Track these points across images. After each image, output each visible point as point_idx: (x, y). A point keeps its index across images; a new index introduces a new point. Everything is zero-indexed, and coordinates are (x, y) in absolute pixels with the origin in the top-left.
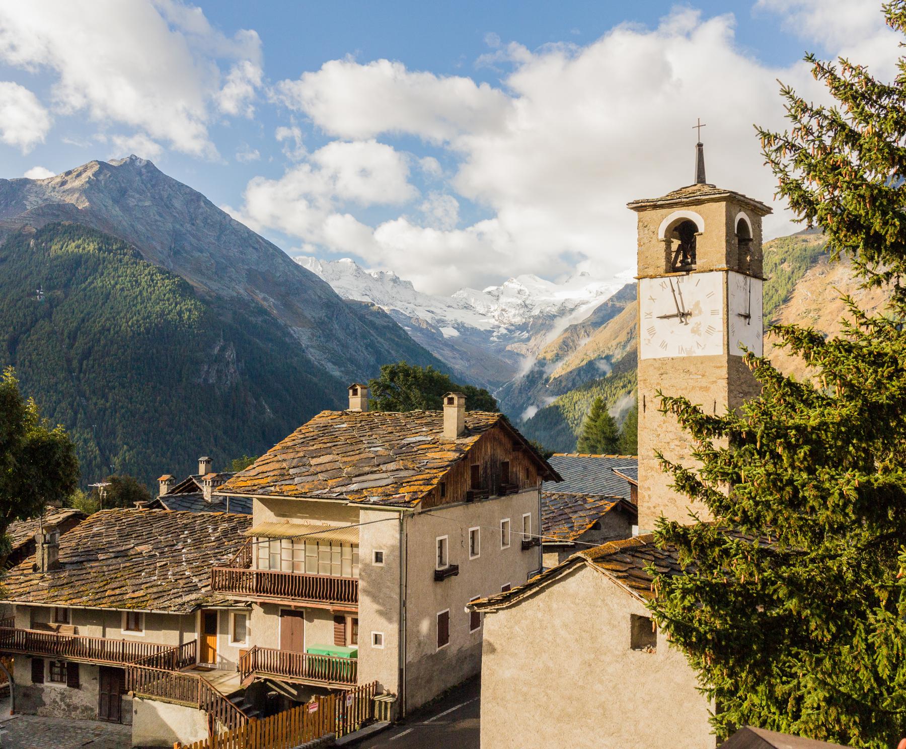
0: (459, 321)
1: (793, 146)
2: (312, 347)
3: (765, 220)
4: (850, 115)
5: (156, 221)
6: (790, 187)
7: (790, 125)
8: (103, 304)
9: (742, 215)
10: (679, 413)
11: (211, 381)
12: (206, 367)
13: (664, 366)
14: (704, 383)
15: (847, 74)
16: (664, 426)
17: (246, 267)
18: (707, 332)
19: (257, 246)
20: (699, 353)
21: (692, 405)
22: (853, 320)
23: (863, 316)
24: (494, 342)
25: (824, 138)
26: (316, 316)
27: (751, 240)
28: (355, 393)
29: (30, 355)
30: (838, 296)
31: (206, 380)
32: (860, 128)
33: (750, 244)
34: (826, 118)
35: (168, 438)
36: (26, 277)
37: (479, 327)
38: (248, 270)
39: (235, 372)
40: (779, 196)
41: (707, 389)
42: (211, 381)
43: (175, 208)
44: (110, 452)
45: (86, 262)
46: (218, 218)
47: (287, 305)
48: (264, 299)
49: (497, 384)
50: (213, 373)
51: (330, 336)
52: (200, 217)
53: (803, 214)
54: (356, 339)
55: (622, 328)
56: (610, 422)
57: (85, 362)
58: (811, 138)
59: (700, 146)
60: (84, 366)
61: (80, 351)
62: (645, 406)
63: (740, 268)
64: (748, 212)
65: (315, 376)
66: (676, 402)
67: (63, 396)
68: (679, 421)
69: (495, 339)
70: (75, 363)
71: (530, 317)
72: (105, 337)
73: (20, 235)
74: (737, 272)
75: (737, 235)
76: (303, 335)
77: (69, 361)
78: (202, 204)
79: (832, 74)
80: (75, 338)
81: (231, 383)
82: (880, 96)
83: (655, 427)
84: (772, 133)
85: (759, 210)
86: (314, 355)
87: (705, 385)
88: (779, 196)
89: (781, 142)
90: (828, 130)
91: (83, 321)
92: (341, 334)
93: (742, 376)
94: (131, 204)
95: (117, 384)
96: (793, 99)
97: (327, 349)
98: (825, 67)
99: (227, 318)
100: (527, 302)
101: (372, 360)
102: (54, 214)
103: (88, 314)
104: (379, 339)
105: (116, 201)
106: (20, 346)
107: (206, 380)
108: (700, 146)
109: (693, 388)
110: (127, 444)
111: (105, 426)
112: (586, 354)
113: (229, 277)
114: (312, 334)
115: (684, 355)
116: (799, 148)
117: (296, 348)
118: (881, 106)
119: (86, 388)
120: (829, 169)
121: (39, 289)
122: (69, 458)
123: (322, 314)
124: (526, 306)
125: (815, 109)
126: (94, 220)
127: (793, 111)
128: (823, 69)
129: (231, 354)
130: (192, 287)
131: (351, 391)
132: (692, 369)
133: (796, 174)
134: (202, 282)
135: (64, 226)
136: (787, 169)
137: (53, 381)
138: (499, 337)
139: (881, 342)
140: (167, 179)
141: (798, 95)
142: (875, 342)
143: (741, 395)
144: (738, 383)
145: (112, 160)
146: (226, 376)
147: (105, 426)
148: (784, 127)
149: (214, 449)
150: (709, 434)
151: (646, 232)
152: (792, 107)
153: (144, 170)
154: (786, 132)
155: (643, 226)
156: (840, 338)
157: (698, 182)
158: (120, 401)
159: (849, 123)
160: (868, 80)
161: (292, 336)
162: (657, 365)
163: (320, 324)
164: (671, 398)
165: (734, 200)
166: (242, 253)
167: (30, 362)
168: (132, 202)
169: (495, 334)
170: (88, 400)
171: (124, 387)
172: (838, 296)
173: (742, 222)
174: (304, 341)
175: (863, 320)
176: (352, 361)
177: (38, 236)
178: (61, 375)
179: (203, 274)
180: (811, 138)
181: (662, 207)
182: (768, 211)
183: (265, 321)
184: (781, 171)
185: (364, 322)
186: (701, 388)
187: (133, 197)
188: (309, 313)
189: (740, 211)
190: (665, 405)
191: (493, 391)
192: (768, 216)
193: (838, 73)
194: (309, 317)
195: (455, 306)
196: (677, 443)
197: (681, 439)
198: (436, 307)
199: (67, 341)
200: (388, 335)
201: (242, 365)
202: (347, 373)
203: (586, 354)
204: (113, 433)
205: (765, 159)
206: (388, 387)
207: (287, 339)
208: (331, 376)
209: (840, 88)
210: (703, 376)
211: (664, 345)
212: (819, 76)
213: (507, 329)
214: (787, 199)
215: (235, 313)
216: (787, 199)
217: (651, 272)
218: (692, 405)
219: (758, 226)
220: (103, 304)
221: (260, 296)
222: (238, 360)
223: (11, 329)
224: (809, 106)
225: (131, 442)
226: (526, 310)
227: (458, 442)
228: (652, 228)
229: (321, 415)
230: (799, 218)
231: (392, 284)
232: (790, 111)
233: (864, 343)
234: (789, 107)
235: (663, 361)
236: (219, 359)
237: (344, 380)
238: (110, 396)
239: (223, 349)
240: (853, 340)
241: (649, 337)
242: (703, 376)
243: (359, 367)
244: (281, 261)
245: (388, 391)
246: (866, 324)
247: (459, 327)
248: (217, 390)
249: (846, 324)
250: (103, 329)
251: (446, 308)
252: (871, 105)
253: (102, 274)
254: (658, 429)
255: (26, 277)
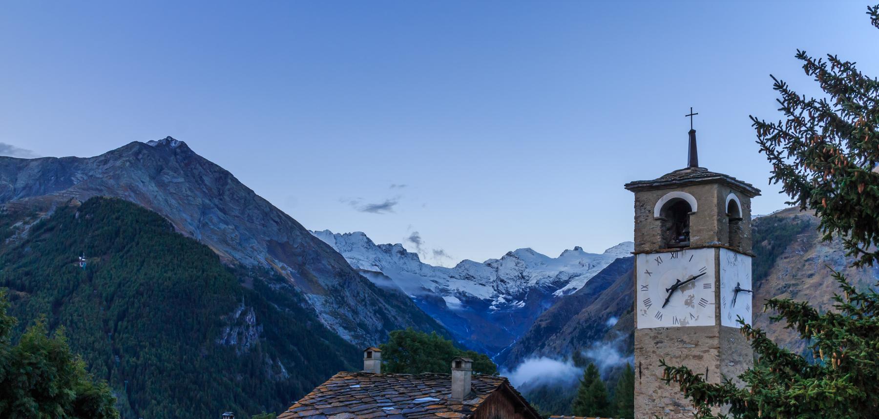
0: (461, 290)
1: (788, 134)
2: (325, 312)
3: (754, 201)
4: (839, 107)
5: (188, 196)
6: (781, 172)
7: (784, 118)
8: (138, 270)
9: (731, 196)
10: (682, 382)
11: (232, 343)
12: (228, 330)
13: (659, 335)
14: (696, 352)
15: (836, 70)
16: (659, 391)
17: (267, 239)
18: (700, 304)
19: (277, 219)
20: (692, 323)
21: (694, 374)
22: (844, 295)
23: (853, 291)
24: (493, 310)
25: (816, 128)
26: (330, 284)
27: (740, 219)
28: (370, 355)
29: (71, 315)
30: (827, 272)
31: (227, 342)
32: (850, 120)
33: (740, 223)
34: (817, 109)
35: (192, 394)
36: (71, 245)
37: (479, 297)
38: (269, 241)
39: (254, 335)
40: (774, 180)
41: (700, 358)
42: (232, 343)
43: (205, 185)
44: (139, 405)
45: (124, 231)
46: (243, 194)
47: (303, 274)
48: (282, 268)
49: (495, 350)
50: (235, 334)
51: (342, 302)
52: (227, 193)
53: (796, 197)
54: (365, 305)
55: (613, 299)
56: (599, 388)
57: (120, 323)
58: (803, 128)
59: (692, 133)
60: (119, 327)
61: (116, 313)
62: (640, 372)
63: (730, 245)
64: (739, 194)
65: (327, 339)
66: (678, 371)
67: (99, 354)
68: (682, 390)
69: (494, 307)
70: (111, 324)
71: (526, 288)
72: (139, 301)
73: (67, 207)
74: (728, 249)
75: (728, 215)
76: (316, 301)
77: (106, 322)
78: (229, 181)
79: (823, 70)
80: (112, 300)
81: (251, 344)
82: (867, 90)
83: (651, 392)
84: (767, 122)
85: (748, 192)
86: (326, 320)
87: (698, 353)
88: (774, 180)
89: (776, 131)
90: (819, 121)
91: (119, 285)
92: (352, 302)
93: (733, 346)
94: (166, 181)
95: (147, 344)
96: (786, 93)
97: (338, 314)
98: (816, 63)
99: (248, 285)
100: (524, 274)
101: (380, 326)
102: (97, 189)
103: (124, 279)
104: (387, 306)
105: (153, 178)
106: (63, 308)
107: (227, 342)
108: (692, 133)
109: (687, 356)
110: (155, 399)
111: (135, 382)
112: (579, 323)
113: (252, 247)
114: (326, 301)
115: (678, 325)
116: (793, 137)
117: (309, 314)
118: (869, 99)
119: (119, 346)
120: (818, 154)
121: (81, 256)
122: (111, 411)
123: (336, 282)
124: (523, 277)
125: (806, 101)
126: (132, 194)
127: (786, 104)
128: (814, 65)
129: (251, 318)
130: (218, 257)
131: (366, 354)
132: (686, 338)
133: (790, 161)
134: (227, 252)
135: (105, 200)
136: (781, 156)
137: (91, 339)
138: (497, 306)
139: (871, 317)
140: (201, 160)
141: (791, 88)
142: (865, 316)
143: (732, 364)
144: (730, 352)
145: (151, 141)
146: (246, 338)
147: (135, 382)
148: (777, 117)
149: (234, 405)
150: (711, 401)
151: (643, 211)
152: (785, 100)
153: (178, 150)
154: (780, 123)
155: (639, 205)
156: (833, 312)
157: (692, 166)
158: (150, 359)
159: (839, 114)
160: (855, 74)
161: (306, 302)
162: (652, 334)
163: (334, 292)
164: (674, 368)
165: (725, 182)
166: (263, 225)
167: (72, 321)
168: (166, 179)
169: (494, 303)
170: (121, 357)
171: (153, 346)
172: (827, 272)
173: (732, 203)
174: (318, 308)
175: (854, 296)
176: (362, 325)
177: (80, 209)
178: (99, 334)
179: (228, 245)
180: (803, 128)
181: (658, 188)
182: (757, 192)
183: (283, 288)
184: (776, 158)
185: (374, 290)
186: (694, 357)
187: (167, 174)
188: (322, 281)
189: (731, 192)
190: (669, 374)
191: (491, 356)
192: (757, 197)
193: (828, 69)
194: (323, 284)
195: (457, 276)
196: (671, 408)
197: (676, 405)
198: (439, 277)
199: (105, 303)
200: (395, 302)
201: (261, 328)
202: (356, 337)
203: (579, 323)
204: (142, 388)
205: (759, 147)
206: (395, 351)
207: (302, 305)
208: (342, 339)
209: (824, 78)
210: (696, 345)
211: (659, 316)
212: (811, 72)
213: (504, 298)
214: (781, 184)
215: (256, 280)
216: (781, 184)
217: (647, 247)
218: (694, 374)
219: (747, 207)
220: (138, 270)
221: (278, 265)
222: (258, 324)
223: (56, 292)
224: (802, 99)
225: (159, 397)
226: (523, 281)
227: (465, 403)
228: (648, 208)
229: (338, 375)
230: (793, 201)
231: (399, 255)
232: (783, 104)
233: (855, 317)
234: (782, 100)
235: (659, 331)
236: (240, 323)
237: (354, 343)
238: (141, 354)
239: (244, 314)
240: (844, 314)
241: (646, 308)
242: (696, 345)
243: (367, 331)
244: (298, 233)
245: (396, 355)
246: (856, 299)
247: (461, 295)
248: (237, 351)
249: (838, 299)
250: (137, 293)
251: (449, 279)
252: (860, 98)
253: (138, 243)
254: (654, 394)
255: (71, 245)
